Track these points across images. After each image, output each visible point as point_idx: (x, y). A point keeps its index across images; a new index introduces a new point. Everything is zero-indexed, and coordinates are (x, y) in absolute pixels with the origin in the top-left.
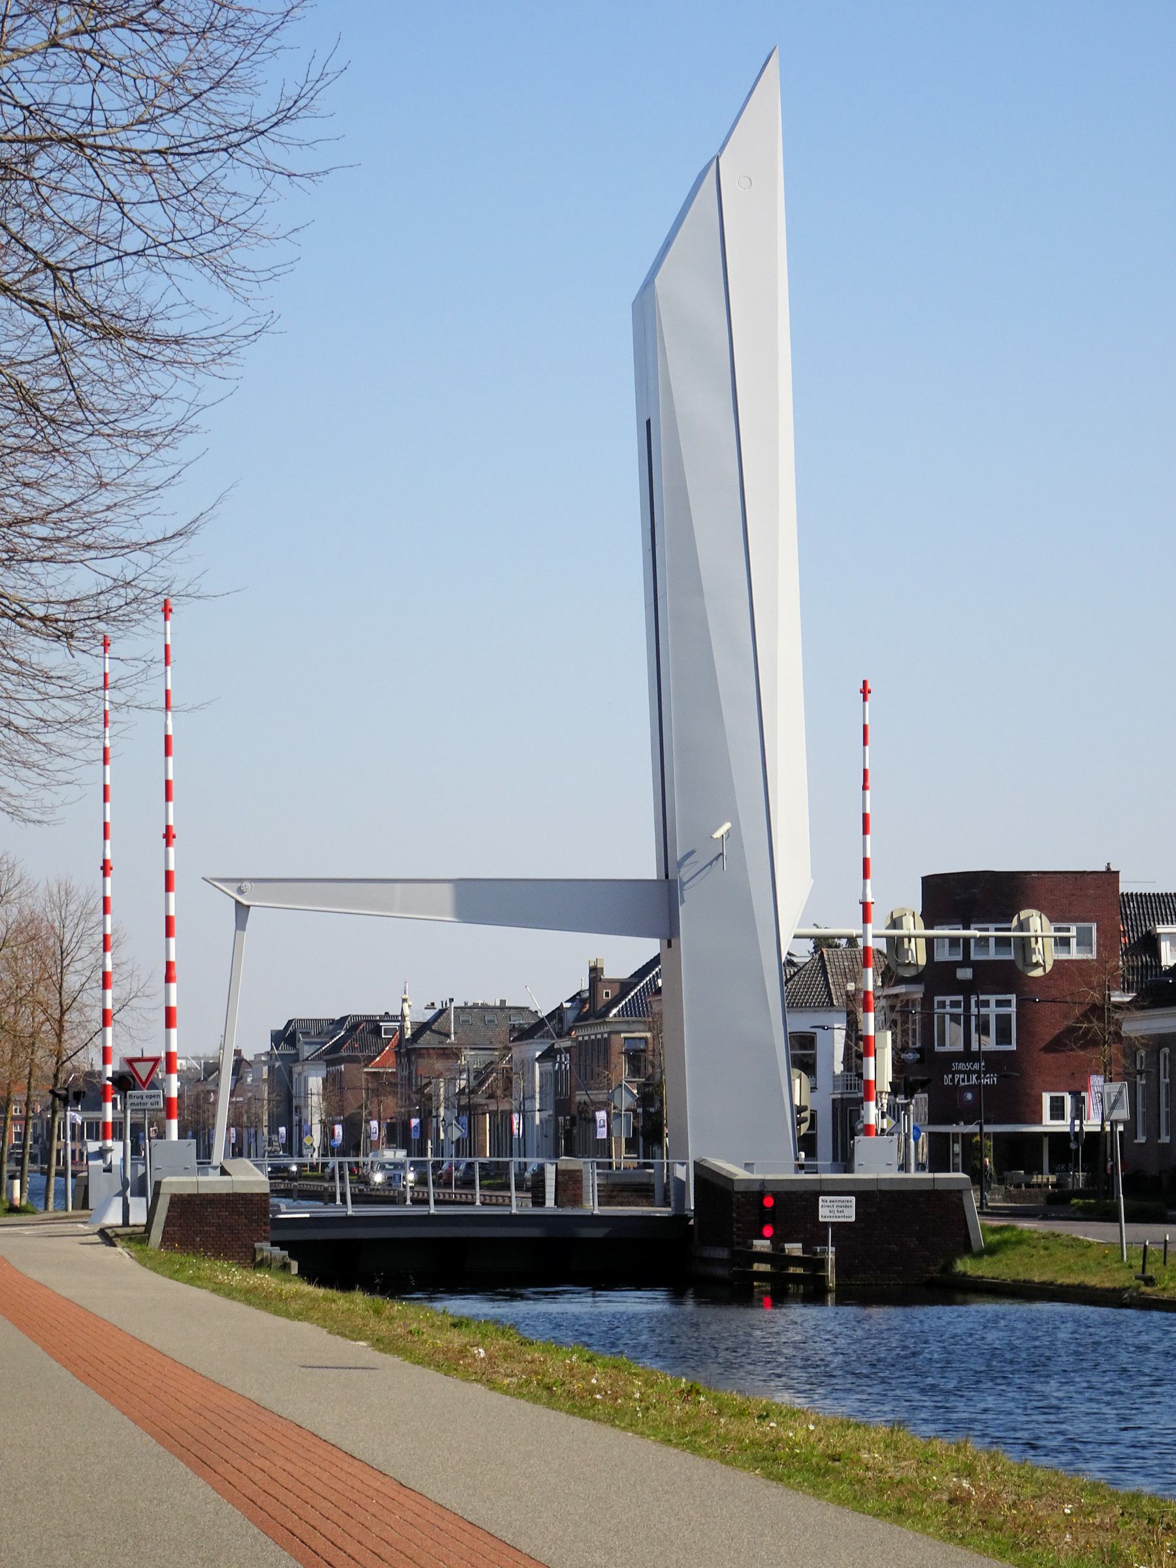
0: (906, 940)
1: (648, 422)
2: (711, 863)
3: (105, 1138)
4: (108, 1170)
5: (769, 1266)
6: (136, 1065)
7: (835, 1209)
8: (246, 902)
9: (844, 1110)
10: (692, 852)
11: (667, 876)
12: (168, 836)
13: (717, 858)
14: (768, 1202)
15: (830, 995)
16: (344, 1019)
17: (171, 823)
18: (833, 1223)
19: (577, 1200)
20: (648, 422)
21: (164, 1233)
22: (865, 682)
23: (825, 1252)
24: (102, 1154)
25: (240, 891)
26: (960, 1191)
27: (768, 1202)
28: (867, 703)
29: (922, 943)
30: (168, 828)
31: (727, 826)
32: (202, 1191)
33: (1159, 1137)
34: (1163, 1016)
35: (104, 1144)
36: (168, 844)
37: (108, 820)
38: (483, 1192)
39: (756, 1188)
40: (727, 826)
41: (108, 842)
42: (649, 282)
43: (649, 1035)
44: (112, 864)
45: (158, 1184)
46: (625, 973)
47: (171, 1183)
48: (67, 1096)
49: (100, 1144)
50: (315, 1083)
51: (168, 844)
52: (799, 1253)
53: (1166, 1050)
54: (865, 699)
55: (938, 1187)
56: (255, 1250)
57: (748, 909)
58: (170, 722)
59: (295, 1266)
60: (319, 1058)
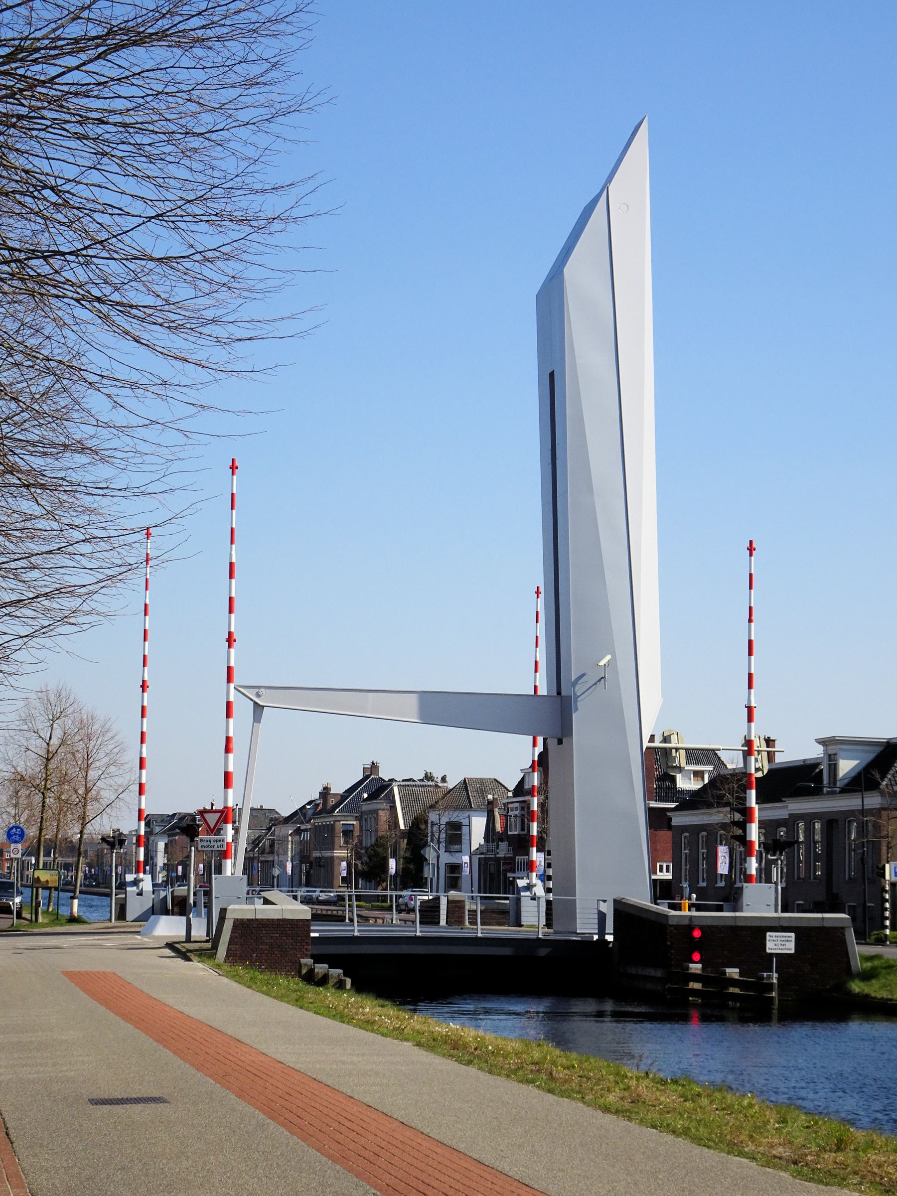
0: (674, 751)
1: (552, 375)
2: (595, 684)
3: (137, 872)
4: (140, 894)
5: (700, 985)
6: (206, 816)
7: (779, 943)
8: (261, 704)
9: (486, 863)
10: (583, 675)
11: (559, 693)
12: (230, 640)
13: (600, 680)
14: (697, 934)
15: (470, 802)
16: (174, 815)
17: (232, 630)
18: (777, 955)
19: (460, 922)
20: (552, 375)
21: (228, 949)
22: (751, 542)
23: (769, 977)
24: (136, 883)
25: (258, 695)
26: (843, 928)
27: (697, 934)
28: (753, 558)
29: (765, 754)
30: (230, 633)
31: (609, 657)
32: (259, 917)
33: (698, 883)
34: (686, 815)
35: (138, 876)
36: (230, 647)
37: (146, 653)
38: (394, 911)
39: (686, 922)
40: (609, 657)
41: (146, 669)
42: (555, 277)
43: (354, 823)
44: (148, 684)
45: (223, 912)
46: (341, 791)
47: (234, 910)
48: (114, 842)
49: (135, 876)
50: (161, 845)
51: (230, 647)
52: (737, 977)
53: (705, 833)
54: (751, 555)
55: (826, 925)
56: (300, 965)
57: (615, 719)
58: (234, 553)
59: (349, 981)
60: (164, 833)
